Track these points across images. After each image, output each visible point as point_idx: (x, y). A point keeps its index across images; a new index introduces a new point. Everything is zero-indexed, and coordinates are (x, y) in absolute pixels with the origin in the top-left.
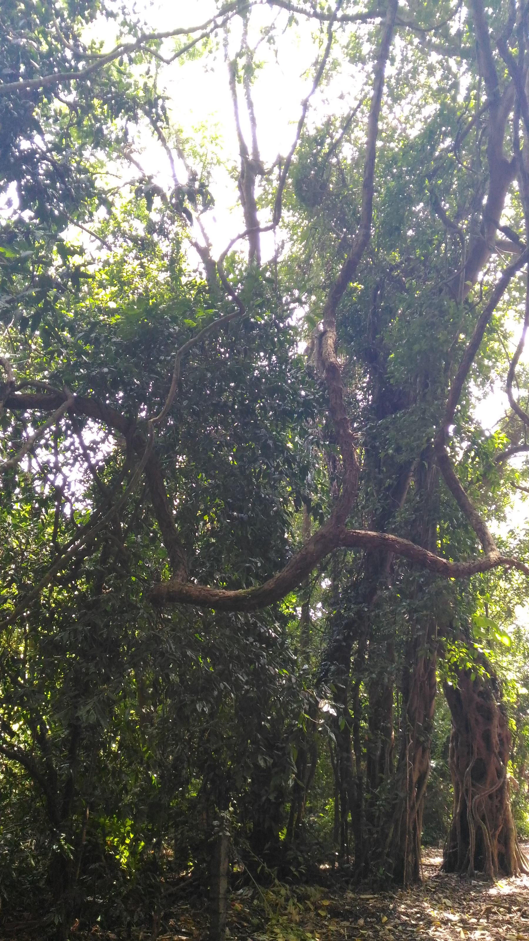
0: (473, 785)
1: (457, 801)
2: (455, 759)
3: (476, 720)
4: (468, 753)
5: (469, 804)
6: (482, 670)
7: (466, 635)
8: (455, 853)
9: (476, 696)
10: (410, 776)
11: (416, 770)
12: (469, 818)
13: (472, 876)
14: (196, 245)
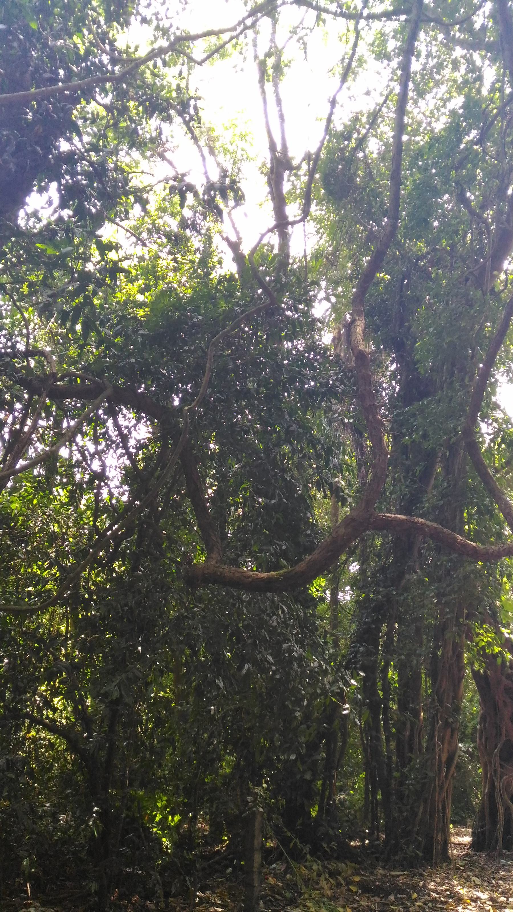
2: (483, 740)
5: (497, 784)
8: (484, 833)
9: (504, 678)
10: (439, 756)
11: (446, 750)
12: (498, 798)
13: (501, 855)
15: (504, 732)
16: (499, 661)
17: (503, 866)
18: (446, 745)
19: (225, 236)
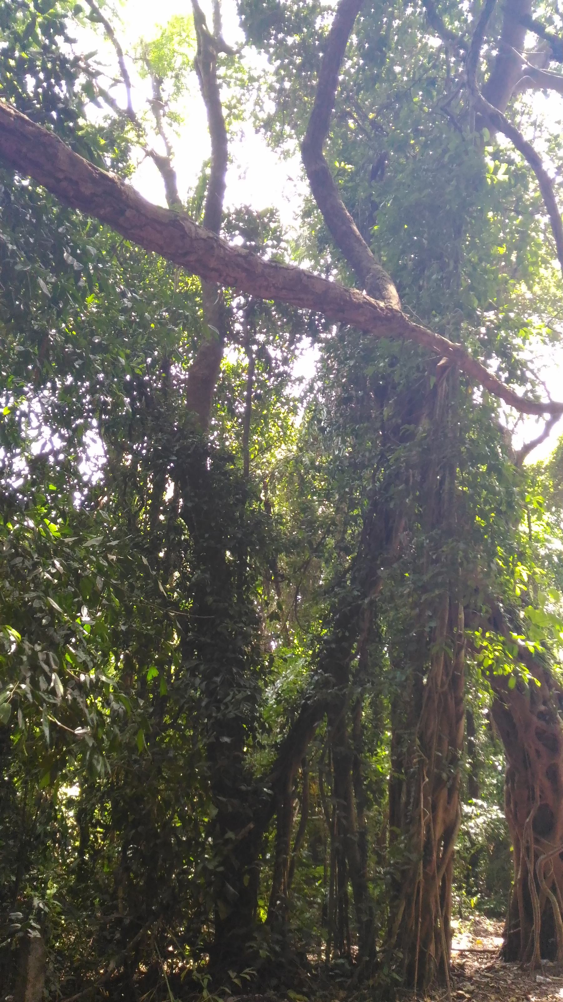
0: (537, 841)
1: (518, 865)
2: (512, 806)
3: (537, 752)
4: (529, 799)
5: (531, 867)
6: (527, 675)
7: (501, 621)
8: (517, 934)
9: (535, 719)
10: (428, 831)
11: (440, 820)
12: (532, 887)
13: (538, 968)
14: (151, 154)
15: (538, 793)
16: (512, 683)
17: (540, 984)
18: (441, 814)
19: (149, 149)
